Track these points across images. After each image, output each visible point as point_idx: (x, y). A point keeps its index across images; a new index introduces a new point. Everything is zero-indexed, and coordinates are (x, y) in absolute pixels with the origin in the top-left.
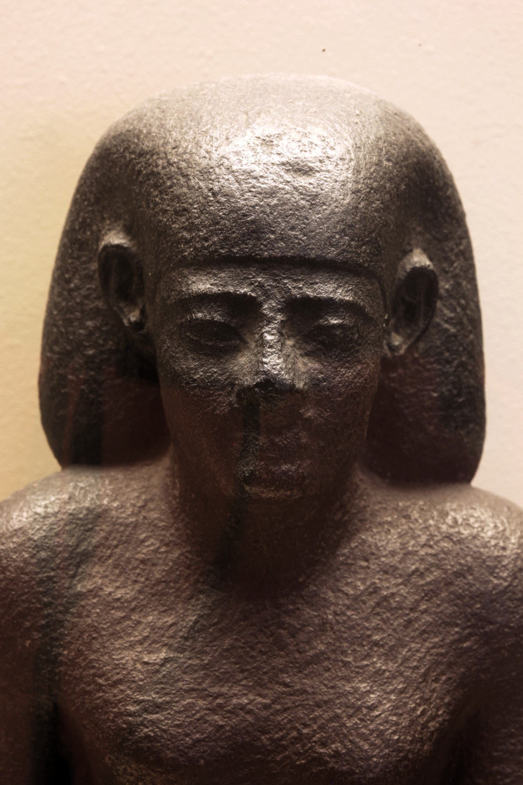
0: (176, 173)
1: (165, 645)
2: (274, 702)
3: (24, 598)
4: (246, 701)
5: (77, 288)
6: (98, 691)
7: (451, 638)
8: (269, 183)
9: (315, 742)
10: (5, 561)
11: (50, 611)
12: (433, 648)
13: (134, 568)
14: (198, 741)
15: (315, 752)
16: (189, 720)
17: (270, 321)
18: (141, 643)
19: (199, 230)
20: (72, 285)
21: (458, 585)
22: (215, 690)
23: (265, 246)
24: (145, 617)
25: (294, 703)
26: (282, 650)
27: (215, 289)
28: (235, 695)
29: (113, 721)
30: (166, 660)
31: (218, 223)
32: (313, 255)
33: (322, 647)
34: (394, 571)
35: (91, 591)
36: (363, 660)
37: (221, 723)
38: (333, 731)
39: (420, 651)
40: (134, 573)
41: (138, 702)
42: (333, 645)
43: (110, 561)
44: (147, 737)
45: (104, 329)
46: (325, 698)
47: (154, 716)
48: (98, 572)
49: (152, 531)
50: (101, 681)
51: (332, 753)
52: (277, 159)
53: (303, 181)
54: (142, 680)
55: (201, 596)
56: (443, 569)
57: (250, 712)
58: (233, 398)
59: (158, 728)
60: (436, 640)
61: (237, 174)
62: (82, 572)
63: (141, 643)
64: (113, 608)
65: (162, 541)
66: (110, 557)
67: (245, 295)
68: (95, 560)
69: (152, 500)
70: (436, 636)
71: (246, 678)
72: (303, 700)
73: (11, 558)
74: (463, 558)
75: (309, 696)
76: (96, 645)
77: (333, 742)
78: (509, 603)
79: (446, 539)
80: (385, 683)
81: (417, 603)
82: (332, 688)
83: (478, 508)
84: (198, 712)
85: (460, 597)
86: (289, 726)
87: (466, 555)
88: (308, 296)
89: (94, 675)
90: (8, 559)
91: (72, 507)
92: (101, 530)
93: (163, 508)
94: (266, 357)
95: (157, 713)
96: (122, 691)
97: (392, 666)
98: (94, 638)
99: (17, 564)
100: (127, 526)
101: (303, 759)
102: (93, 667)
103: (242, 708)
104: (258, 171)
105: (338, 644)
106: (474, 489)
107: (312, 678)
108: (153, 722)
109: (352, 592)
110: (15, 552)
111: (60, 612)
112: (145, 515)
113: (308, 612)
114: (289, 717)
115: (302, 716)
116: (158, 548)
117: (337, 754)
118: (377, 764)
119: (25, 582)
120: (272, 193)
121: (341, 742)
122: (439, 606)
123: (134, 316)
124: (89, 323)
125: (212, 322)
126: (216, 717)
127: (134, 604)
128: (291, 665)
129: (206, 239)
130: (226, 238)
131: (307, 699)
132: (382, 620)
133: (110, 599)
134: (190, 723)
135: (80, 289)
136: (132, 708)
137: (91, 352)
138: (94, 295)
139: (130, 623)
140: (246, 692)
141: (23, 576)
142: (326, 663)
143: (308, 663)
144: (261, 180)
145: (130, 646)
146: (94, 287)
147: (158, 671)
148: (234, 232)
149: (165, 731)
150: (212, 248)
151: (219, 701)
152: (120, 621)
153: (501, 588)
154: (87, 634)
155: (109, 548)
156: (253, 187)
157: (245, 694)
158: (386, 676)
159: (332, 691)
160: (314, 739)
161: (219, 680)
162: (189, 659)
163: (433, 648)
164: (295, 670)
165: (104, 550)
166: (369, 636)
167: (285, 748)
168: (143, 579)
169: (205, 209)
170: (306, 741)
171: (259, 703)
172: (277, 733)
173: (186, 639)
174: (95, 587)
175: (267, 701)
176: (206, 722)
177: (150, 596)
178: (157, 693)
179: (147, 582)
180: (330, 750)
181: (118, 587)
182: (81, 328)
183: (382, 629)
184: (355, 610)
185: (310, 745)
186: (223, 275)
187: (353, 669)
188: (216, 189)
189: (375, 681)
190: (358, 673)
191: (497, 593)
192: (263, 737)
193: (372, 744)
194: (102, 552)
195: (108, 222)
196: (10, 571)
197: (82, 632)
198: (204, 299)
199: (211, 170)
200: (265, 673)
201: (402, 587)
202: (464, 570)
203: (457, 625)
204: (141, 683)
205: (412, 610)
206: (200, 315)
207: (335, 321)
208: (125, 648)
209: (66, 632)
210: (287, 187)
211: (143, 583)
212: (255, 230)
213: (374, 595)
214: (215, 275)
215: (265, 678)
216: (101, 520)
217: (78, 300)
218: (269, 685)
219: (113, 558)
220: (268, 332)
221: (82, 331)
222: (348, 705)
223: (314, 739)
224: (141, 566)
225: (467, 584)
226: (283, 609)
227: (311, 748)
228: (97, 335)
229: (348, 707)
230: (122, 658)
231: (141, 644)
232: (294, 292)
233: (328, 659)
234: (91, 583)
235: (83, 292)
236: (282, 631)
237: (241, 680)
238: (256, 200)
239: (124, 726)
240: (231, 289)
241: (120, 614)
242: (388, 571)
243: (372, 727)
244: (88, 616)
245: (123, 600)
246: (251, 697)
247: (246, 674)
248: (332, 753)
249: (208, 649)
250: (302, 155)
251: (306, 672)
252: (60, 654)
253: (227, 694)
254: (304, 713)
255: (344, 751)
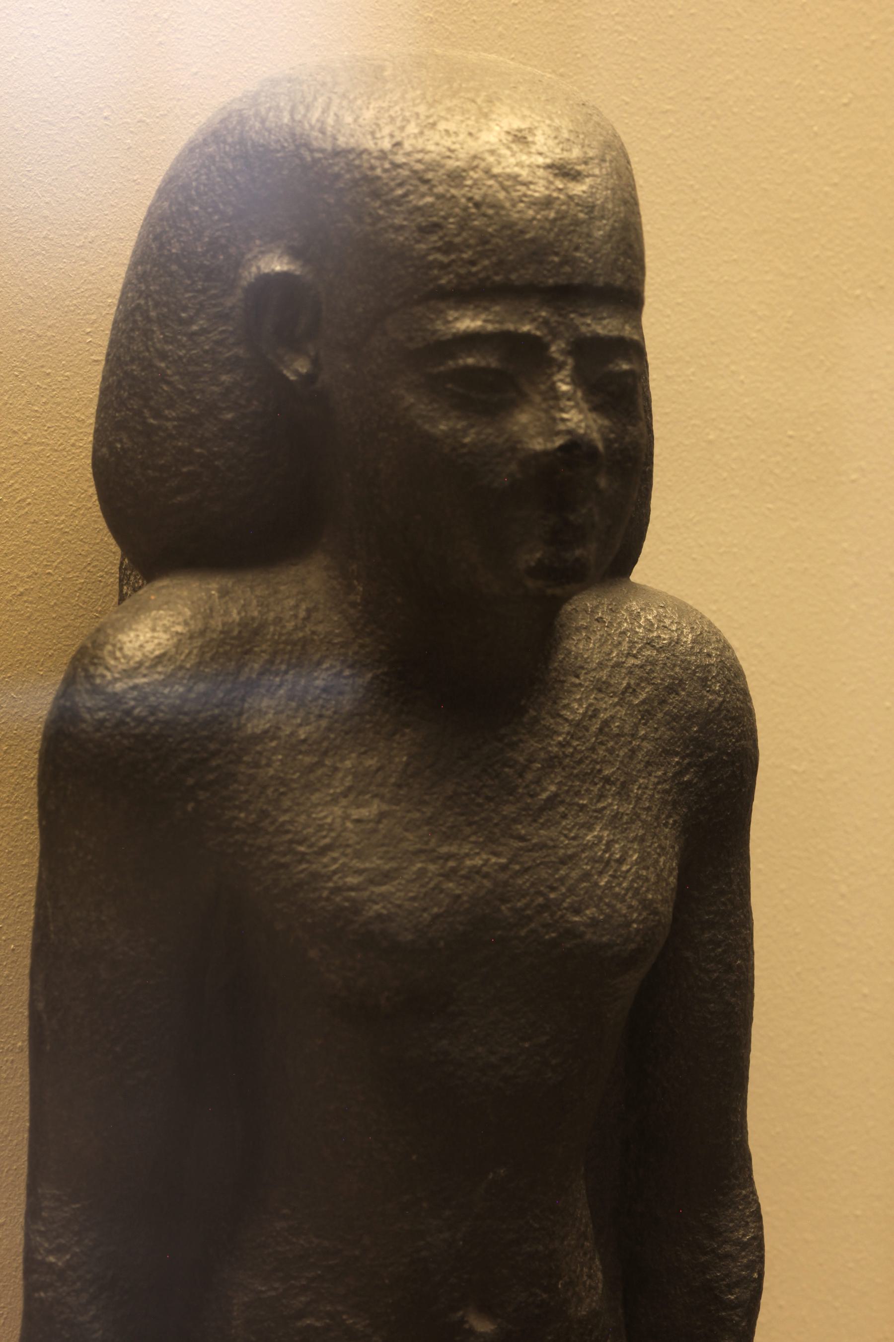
0: (409, 177)
1: (375, 796)
2: (511, 861)
3: (185, 745)
4: (480, 862)
5: (203, 331)
6: (300, 862)
7: (673, 770)
8: (539, 190)
9: (566, 909)
10: (152, 699)
11: (219, 762)
12: (658, 783)
13: (316, 699)
14: (436, 917)
15: (567, 921)
16: (423, 890)
17: (561, 366)
18: (345, 795)
19: (462, 252)
20: (195, 328)
21: (672, 703)
22: (444, 849)
23: (549, 271)
24: (342, 760)
25: (534, 860)
26: (511, 794)
27: (490, 327)
28: (467, 855)
29: (328, 899)
30: (382, 815)
31: (487, 242)
32: (601, 281)
33: (553, 788)
34: (607, 687)
35: (266, 732)
36: (598, 801)
37: (458, 892)
38: (586, 893)
39: (649, 785)
40: (316, 706)
41: (359, 872)
42: (565, 785)
43: (282, 692)
44: (379, 916)
45: (247, 384)
46: (569, 852)
47: (383, 889)
48: (269, 707)
49: (327, 650)
50: (302, 849)
51: (589, 921)
52: (541, 160)
53: (579, 189)
54: (358, 843)
55: (407, 731)
56: (653, 684)
57: (486, 876)
58: (513, 467)
59: (391, 903)
60: (660, 773)
61: (500, 179)
62: (250, 708)
63: (345, 795)
64: (300, 752)
65: (343, 662)
66: (280, 686)
67: (527, 335)
68: (263, 691)
69: (316, 609)
70: (659, 769)
71: (475, 833)
72: (545, 857)
73: (162, 694)
74: (672, 670)
75: (550, 851)
76: (286, 803)
77: (587, 908)
78: (725, 724)
79: (648, 646)
80: (626, 829)
81: (636, 726)
82: (574, 838)
83: (166, 642)
84: (431, 879)
85: (676, 718)
86: (532, 890)
87: (675, 665)
88: (598, 334)
89: (291, 842)
90: (158, 695)
91: (217, 623)
92: (262, 651)
93: (336, 619)
94: (566, 412)
95: (385, 884)
96: (335, 860)
97: (627, 808)
98: (283, 794)
99: (170, 701)
100: (294, 644)
101: (553, 932)
102: (287, 832)
103: (477, 870)
104: (524, 173)
105: (570, 783)
106: (634, 586)
107: (549, 828)
108: (383, 897)
109: (571, 717)
110: (165, 686)
111: (231, 762)
112: (313, 629)
113: (534, 744)
114: (532, 879)
115: (546, 876)
116: (341, 672)
117: (594, 923)
118: (638, 930)
119: (186, 725)
120: (547, 202)
121: (597, 906)
122: (657, 729)
123: (302, 366)
124: (224, 378)
125: (486, 370)
126: (451, 885)
127: (325, 744)
128: (524, 813)
129: (473, 263)
130: (501, 263)
131: (548, 855)
132: (607, 750)
133: (294, 740)
134: (426, 894)
135: (209, 332)
136: (352, 880)
137: (229, 416)
138: (231, 340)
139: (325, 769)
140: (477, 851)
141: (181, 717)
142: (562, 809)
143: (542, 810)
144: (532, 187)
145: (332, 800)
146: (231, 329)
147: (375, 831)
148: (510, 254)
149: (399, 906)
150: (481, 275)
151: (451, 863)
152: (311, 768)
153: (716, 705)
154: (272, 789)
155: (277, 675)
156: (525, 195)
157: (478, 854)
158: (624, 820)
159: (575, 843)
160: (565, 905)
161: (447, 838)
162: (409, 811)
163: (658, 783)
164: (530, 819)
165: (271, 678)
166: (600, 771)
167: (530, 919)
168: (329, 713)
169: (466, 224)
170: (555, 909)
171: (495, 864)
172: (519, 900)
173: (400, 786)
174: (271, 727)
175: (503, 861)
176: (442, 891)
177: (342, 734)
178: (381, 858)
179: (336, 716)
180: (585, 918)
181: (300, 725)
182: (213, 385)
183: (610, 762)
184: (579, 739)
185: (560, 913)
186: (497, 308)
187: (591, 813)
188: (477, 198)
189: (616, 828)
190: (596, 818)
191: (713, 712)
192: (503, 908)
193: (630, 907)
194: (269, 680)
195: (258, 242)
196: (162, 711)
197: (265, 787)
198: (471, 340)
199: (464, 174)
200: (496, 825)
201: (618, 708)
202: (676, 685)
203: (677, 754)
204: (358, 847)
205: (633, 736)
206: (470, 361)
207: (625, 367)
208: (326, 804)
209: (242, 788)
210: (562, 197)
211: (330, 717)
212: (538, 251)
213: (594, 720)
214: (486, 309)
215: (496, 830)
216: (258, 638)
217: (207, 347)
218: (502, 840)
219: (285, 688)
220: (562, 381)
221: (214, 388)
222: (597, 859)
223: (565, 905)
224: (324, 696)
225: (681, 702)
226: (506, 741)
227: (562, 917)
228: (238, 393)
229: (596, 862)
230: (325, 817)
231: (346, 796)
232: (583, 329)
233: (562, 802)
234: (263, 722)
235: (215, 336)
236: (507, 770)
237: (469, 836)
238: (531, 212)
239: (347, 904)
240: (510, 327)
241: (308, 760)
242: (601, 687)
243: (625, 885)
244: (268, 765)
245: (310, 742)
246: (485, 856)
247: (474, 827)
248: (589, 921)
249: (427, 798)
250: (565, 155)
251: (541, 821)
252: (235, 818)
253: (458, 854)
254: (547, 873)
255: (601, 917)
